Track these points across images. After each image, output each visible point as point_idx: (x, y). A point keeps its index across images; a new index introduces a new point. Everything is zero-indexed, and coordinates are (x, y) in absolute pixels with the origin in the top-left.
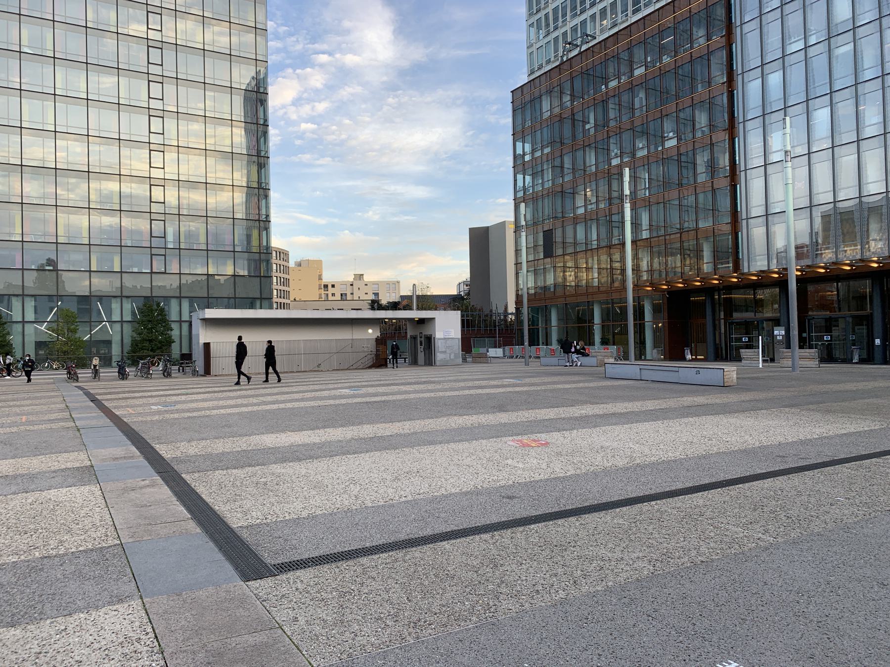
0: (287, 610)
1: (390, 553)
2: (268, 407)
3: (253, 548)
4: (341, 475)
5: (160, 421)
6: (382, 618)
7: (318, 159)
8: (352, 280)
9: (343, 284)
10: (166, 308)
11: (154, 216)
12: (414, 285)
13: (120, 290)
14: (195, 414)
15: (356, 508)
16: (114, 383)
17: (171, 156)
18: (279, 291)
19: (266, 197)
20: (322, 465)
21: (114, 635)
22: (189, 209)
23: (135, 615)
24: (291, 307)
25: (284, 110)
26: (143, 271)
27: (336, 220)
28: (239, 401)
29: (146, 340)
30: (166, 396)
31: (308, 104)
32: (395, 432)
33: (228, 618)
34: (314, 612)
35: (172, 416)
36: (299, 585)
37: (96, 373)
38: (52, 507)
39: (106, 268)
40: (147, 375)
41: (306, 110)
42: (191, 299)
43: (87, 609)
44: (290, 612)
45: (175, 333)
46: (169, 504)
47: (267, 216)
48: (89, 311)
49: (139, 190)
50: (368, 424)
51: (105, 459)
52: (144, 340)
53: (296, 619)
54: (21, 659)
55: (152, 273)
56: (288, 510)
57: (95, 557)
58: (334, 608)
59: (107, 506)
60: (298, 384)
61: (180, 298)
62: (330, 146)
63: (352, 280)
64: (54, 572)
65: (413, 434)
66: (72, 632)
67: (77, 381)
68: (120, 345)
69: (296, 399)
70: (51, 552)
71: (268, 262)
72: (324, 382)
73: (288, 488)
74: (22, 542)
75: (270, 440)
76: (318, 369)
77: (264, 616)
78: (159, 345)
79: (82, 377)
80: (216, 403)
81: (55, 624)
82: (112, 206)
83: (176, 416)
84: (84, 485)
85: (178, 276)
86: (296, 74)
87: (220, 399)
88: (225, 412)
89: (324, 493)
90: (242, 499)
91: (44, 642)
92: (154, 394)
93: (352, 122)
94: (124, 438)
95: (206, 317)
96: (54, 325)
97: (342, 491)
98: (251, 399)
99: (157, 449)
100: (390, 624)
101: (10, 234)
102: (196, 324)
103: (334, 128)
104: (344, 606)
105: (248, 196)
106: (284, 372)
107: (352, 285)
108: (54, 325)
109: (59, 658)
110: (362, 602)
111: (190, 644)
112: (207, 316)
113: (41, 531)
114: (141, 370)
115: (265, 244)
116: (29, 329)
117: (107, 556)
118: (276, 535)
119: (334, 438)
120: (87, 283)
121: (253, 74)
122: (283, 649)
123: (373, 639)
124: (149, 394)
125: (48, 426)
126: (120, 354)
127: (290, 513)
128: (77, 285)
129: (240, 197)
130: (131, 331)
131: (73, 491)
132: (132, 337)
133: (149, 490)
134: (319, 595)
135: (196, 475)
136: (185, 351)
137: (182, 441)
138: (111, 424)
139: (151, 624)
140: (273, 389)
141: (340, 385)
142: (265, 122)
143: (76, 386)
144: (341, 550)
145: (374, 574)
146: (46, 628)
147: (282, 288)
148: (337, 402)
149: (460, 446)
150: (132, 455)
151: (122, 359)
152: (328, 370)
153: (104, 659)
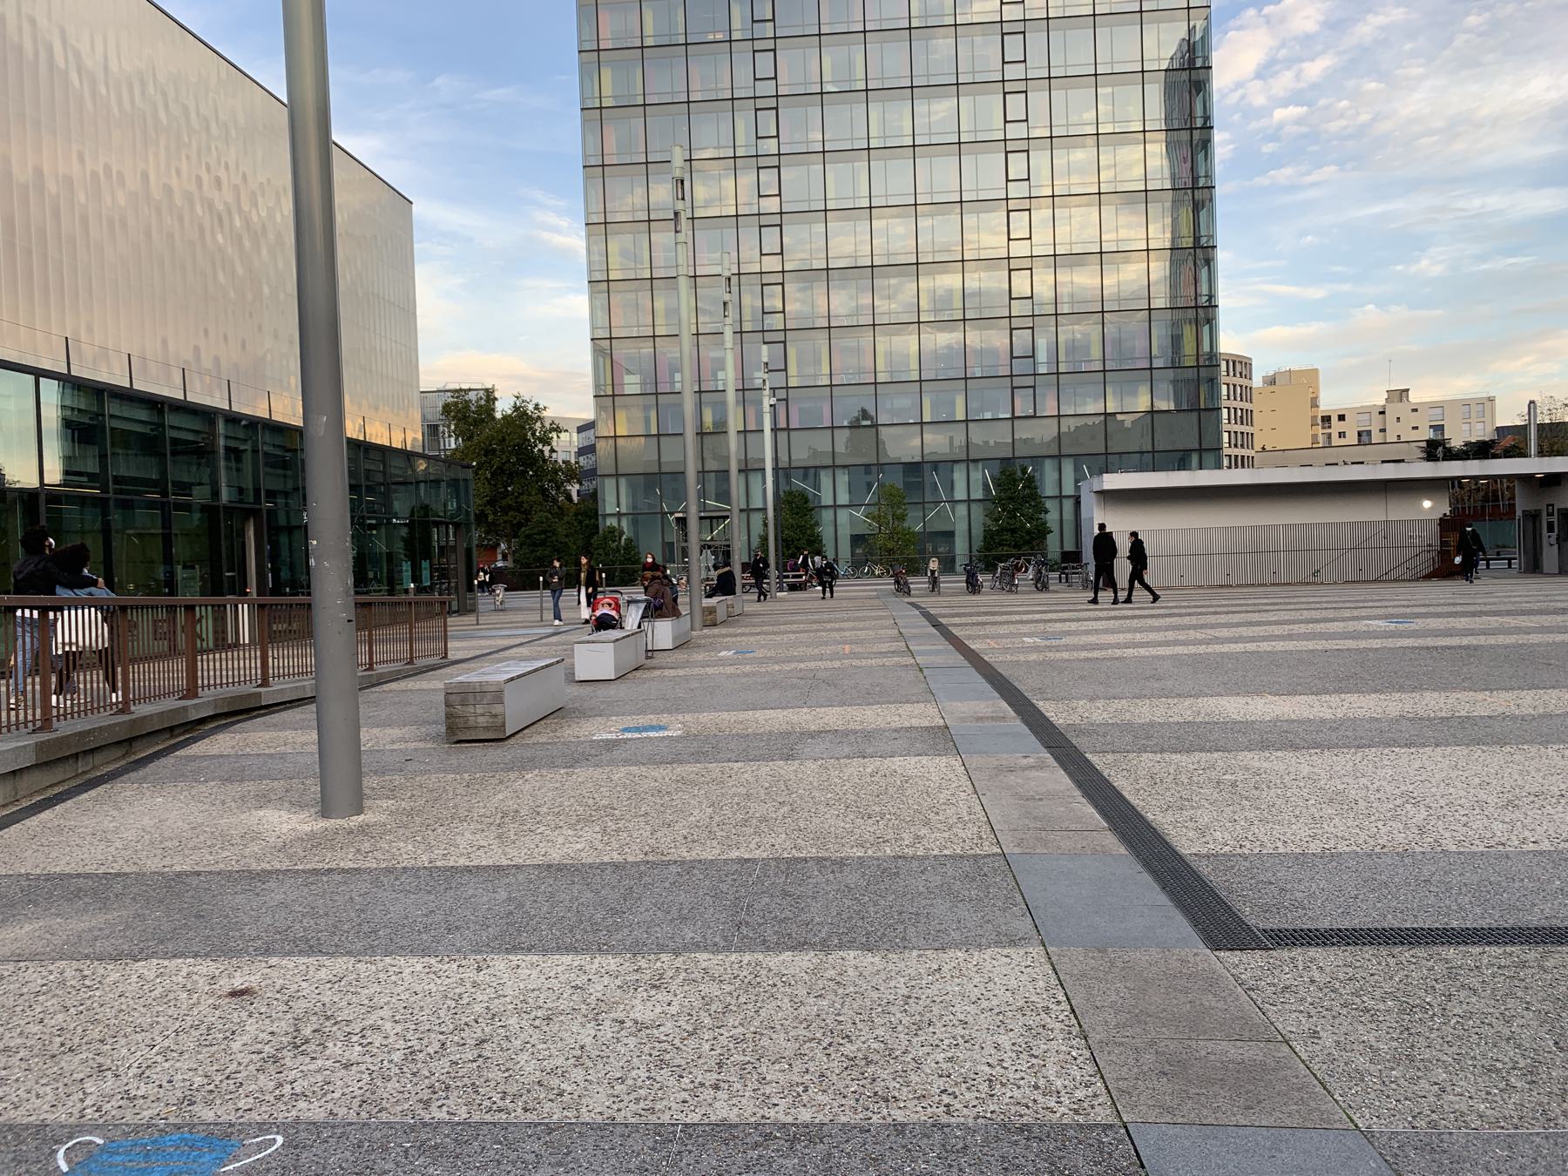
0: (1296, 1014)
1: (1509, 949)
2: (1225, 648)
3: (1223, 894)
4: (1385, 784)
5: (1041, 663)
6: (1498, 1071)
7: (1309, 173)
8: (1384, 403)
9: (1364, 411)
10: (1037, 475)
11: (1016, 323)
12: (1532, 402)
13: (965, 449)
14: (1096, 654)
15: (1421, 849)
16: (961, 598)
17: (1041, 214)
18: (1233, 435)
19: (1209, 262)
20: (1343, 761)
21: (1008, 994)
22: (1072, 303)
23: (1037, 970)
24: (1255, 463)
25: (1240, 92)
26: (1001, 416)
27: (1346, 287)
28: (1170, 635)
29: (1007, 530)
30: (1046, 621)
31: (1289, 68)
32: (1500, 710)
33: (1188, 1006)
34: (1350, 1028)
35: (1058, 655)
36: (1316, 975)
37: (934, 582)
38: (899, 782)
39: (944, 417)
40: (1011, 587)
41: (1285, 81)
42: (1078, 459)
43: (967, 944)
44: (1304, 1020)
45: (1052, 518)
46: (1070, 800)
47: (1211, 297)
48: (920, 486)
49: (989, 281)
50: (1434, 690)
51: (965, 718)
52: (1002, 530)
53: (1315, 1034)
54: (885, 1001)
55: (1014, 418)
56: (1281, 837)
57: (968, 869)
58: (1391, 1030)
59: (976, 792)
60: (1277, 607)
61: (1059, 457)
62: (1335, 143)
63: (1384, 403)
64: (914, 881)
65: (1542, 716)
66: (949, 977)
67: (909, 593)
68: (967, 539)
69: (1278, 636)
70: (907, 850)
71: (1213, 382)
72: (1329, 606)
73: (1278, 796)
74: (867, 829)
75: (1234, 707)
76: (1314, 579)
77: (1253, 1015)
78: (1027, 538)
79: (916, 589)
80: (1129, 636)
81: (924, 959)
82: (952, 315)
83: (1065, 655)
84: (939, 755)
85: (1056, 420)
86: (1265, 16)
87: (1136, 630)
88: (1147, 654)
89: (1352, 815)
90: (1192, 807)
91: (913, 983)
92: (1025, 617)
93: (1382, 85)
94: (988, 686)
95: (1105, 488)
96: (874, 510)
97: (1389, 815)
98: (1192, 632)
99: (1041, 709)
100: (1519, 1085)
101: (815, 376)
102: (1088, 501)
103: (1344, 103)
104: (1413, 1031)
105: (1175, 264)
106: (1168, 588)
107: (1382, 413)
108: (874, 510)
109: (936, 1009)
110: (1452, 1030)
111: (1128, 1034)
112: (1106, 486)
113: (888, 816)
114: (1000, 579)
115: (1206, 348)
116: (843, 515)
117: (985, 869)
118: (1262, 877)
119: (1361, 713)
120: (917, 442)
121: (1183, 34)
122: (1295, 1080)
123: (1483, 1106)
124: (1017, 618)
125: (879, 661)
126: (967, 552)
127: (1285, 842)
128: (903, 447)
129: (1160, 269)
130: (982, 517)
131: (924, 762)
132: (984, 524)
133: (1034, 773)
134: (1358, 1000)
135: (1110, 757)
136: (1069, 547)
137: (1080, 699)
138: (966, 663)
139: (1063, 988)
140: (1230, 615)
141: (1364, 612)
142: (1205, 123)
143: (909, 603)
144: (1396, 925)
145: (1474, 982)
146: (912, 963)
147: (1239, 428)
148: (1363, 644)
149: (85, 796)
150: (1002, 715)
151: (971, 561)
152: (1335, 583)
153: (998, 1027)
